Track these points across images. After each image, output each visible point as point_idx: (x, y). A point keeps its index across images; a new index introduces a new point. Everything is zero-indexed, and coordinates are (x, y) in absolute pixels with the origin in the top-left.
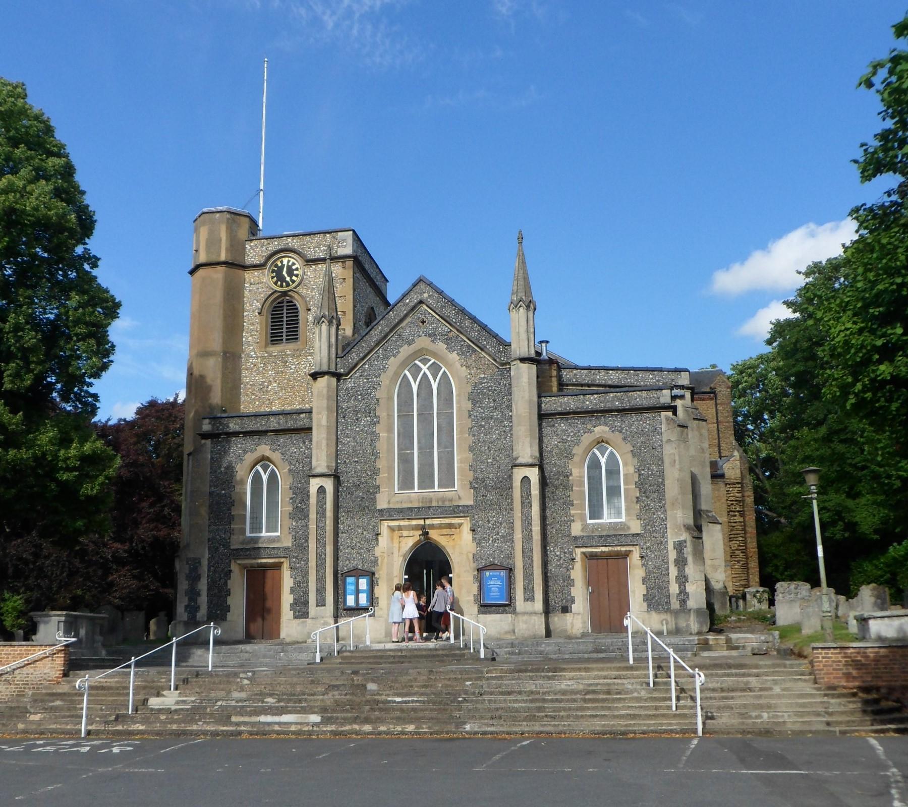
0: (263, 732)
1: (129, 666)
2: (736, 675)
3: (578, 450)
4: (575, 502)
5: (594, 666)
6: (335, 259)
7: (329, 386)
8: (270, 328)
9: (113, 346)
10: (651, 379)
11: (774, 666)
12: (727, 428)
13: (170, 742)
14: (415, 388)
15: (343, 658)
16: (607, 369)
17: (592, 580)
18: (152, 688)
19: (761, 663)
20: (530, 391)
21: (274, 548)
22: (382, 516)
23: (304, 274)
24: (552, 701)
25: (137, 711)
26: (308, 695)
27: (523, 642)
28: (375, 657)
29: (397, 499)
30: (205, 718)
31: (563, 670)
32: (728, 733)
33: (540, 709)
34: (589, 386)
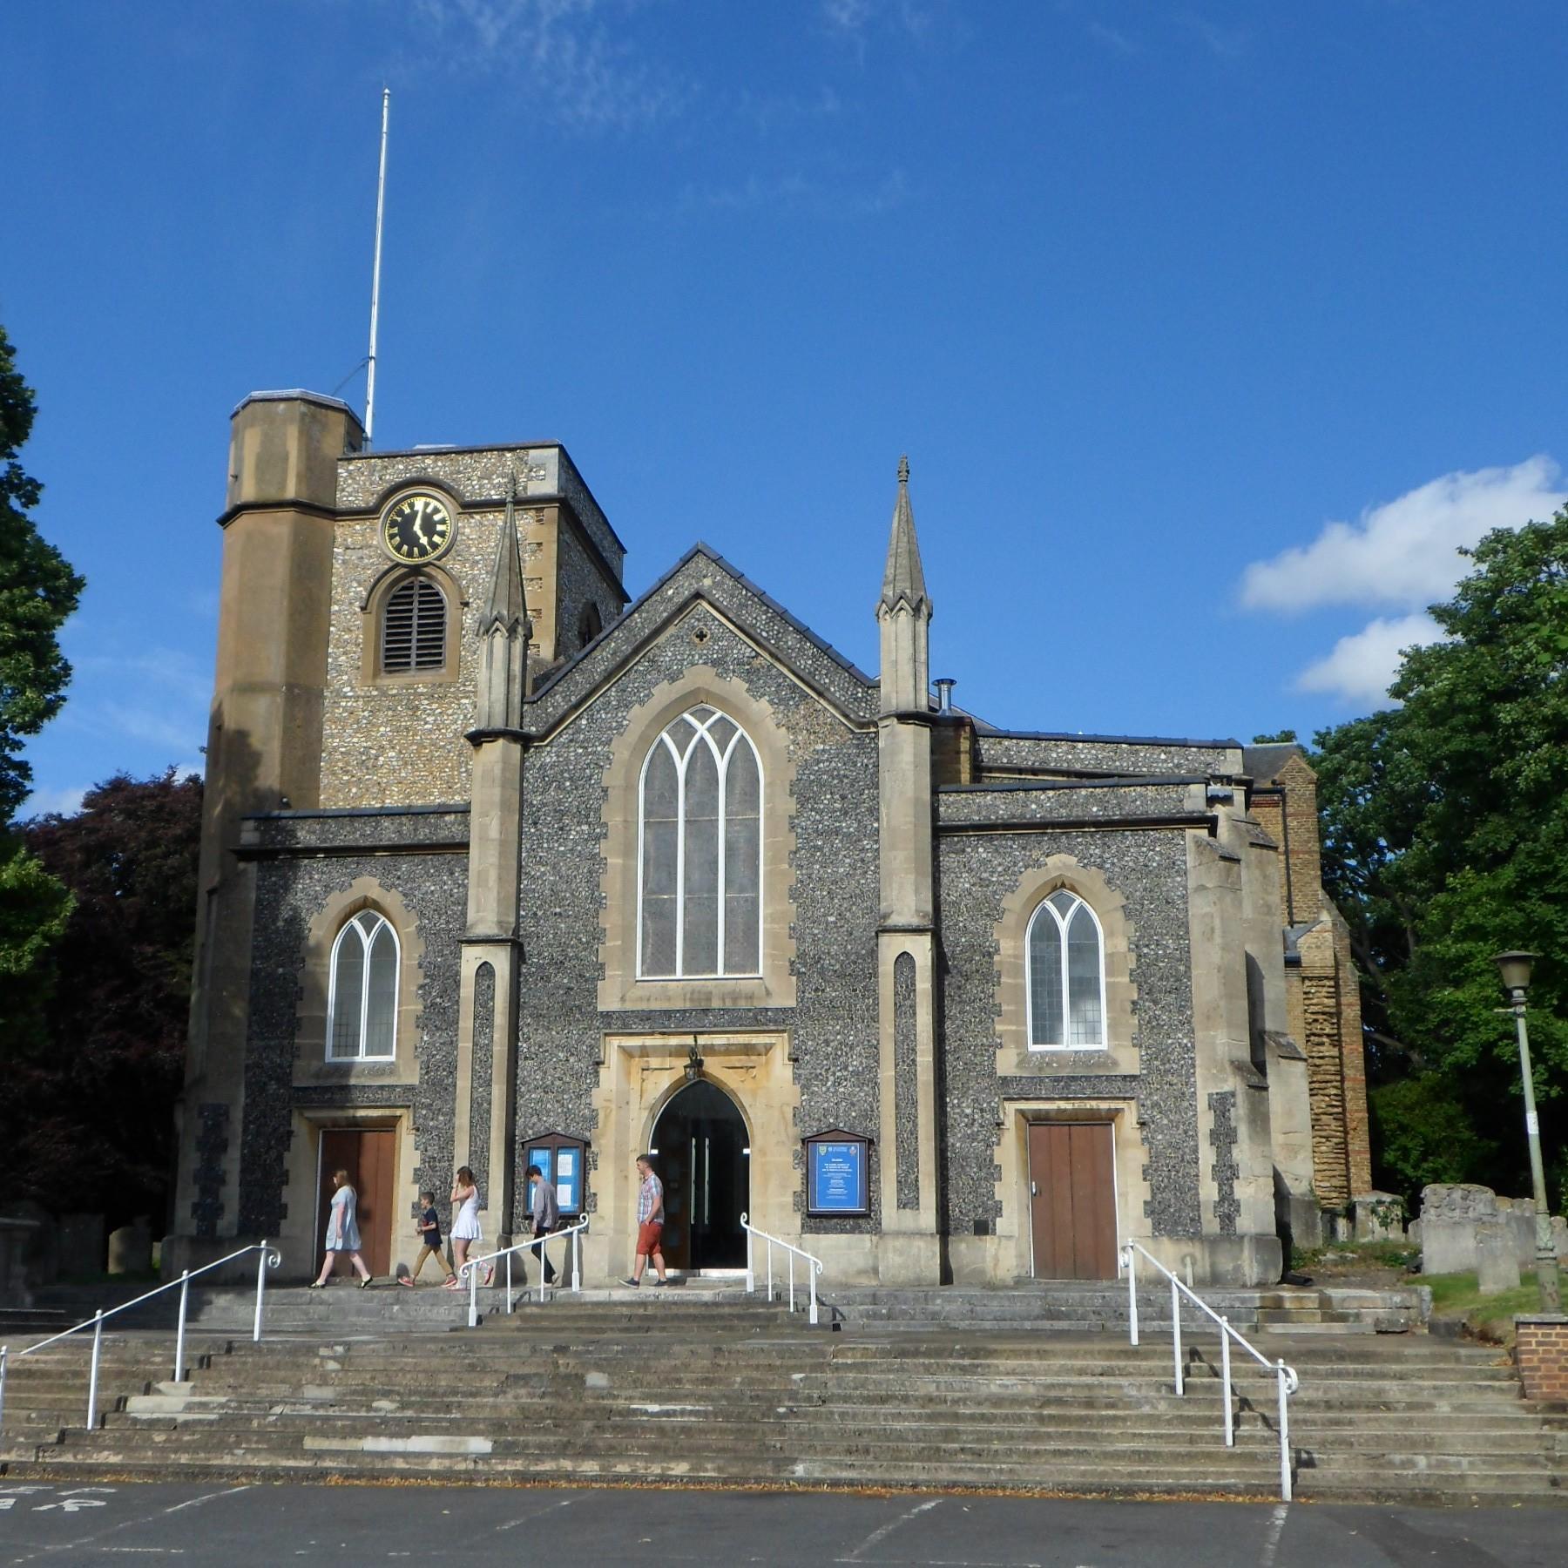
0: (371, 1472)
1: (91, 1328)
2: (1357, 1375)
5: (1058, 1346)
6: (522, 503)
7: (505, 761)
8: (383, 638)
9: (67, 668)
10: (1162, 762)
11: (1435, 1358)
12: (1305, 864)
13: (170, 1489)
14: (681, 767)
15: (524, 1318)
16: (1074, 740)
17: (1039, 1170)
18: (134, 1375)
19: (1408, 1351)
21: (382, 1087)
23: (457, 533)
24: (972, 1418)
25: (103, 1423)
26: (465, 1395)
27: (896, 1292)
28: (591, 1317)
30: (248, 1441)
31: (991, 1354)
32: (1347, 1497)
33: (948, 1435)
34: (1034, 772)
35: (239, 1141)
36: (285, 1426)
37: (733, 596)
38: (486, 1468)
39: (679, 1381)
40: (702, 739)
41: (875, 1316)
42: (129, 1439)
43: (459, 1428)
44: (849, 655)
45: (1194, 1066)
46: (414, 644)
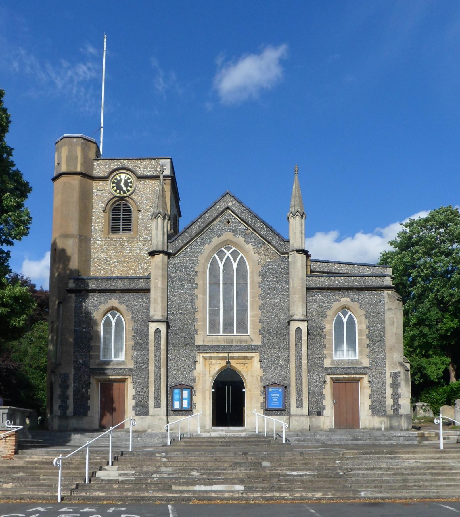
3: (329, 313)
4: (327, 346)
7: (163, 261)
8: (111, 221)
15: (185, 442)
16: (340, 263)
17: (336, 396)
21: (121, 369)
22: (199, 350)
29: (209, 339)
35: (73, 385)
37: (239, 209)
39: (296, 464)
40: (228, 257)
41: (299, 441)
43: (227, 482)
44: (278, 231)
45: (385, 364)
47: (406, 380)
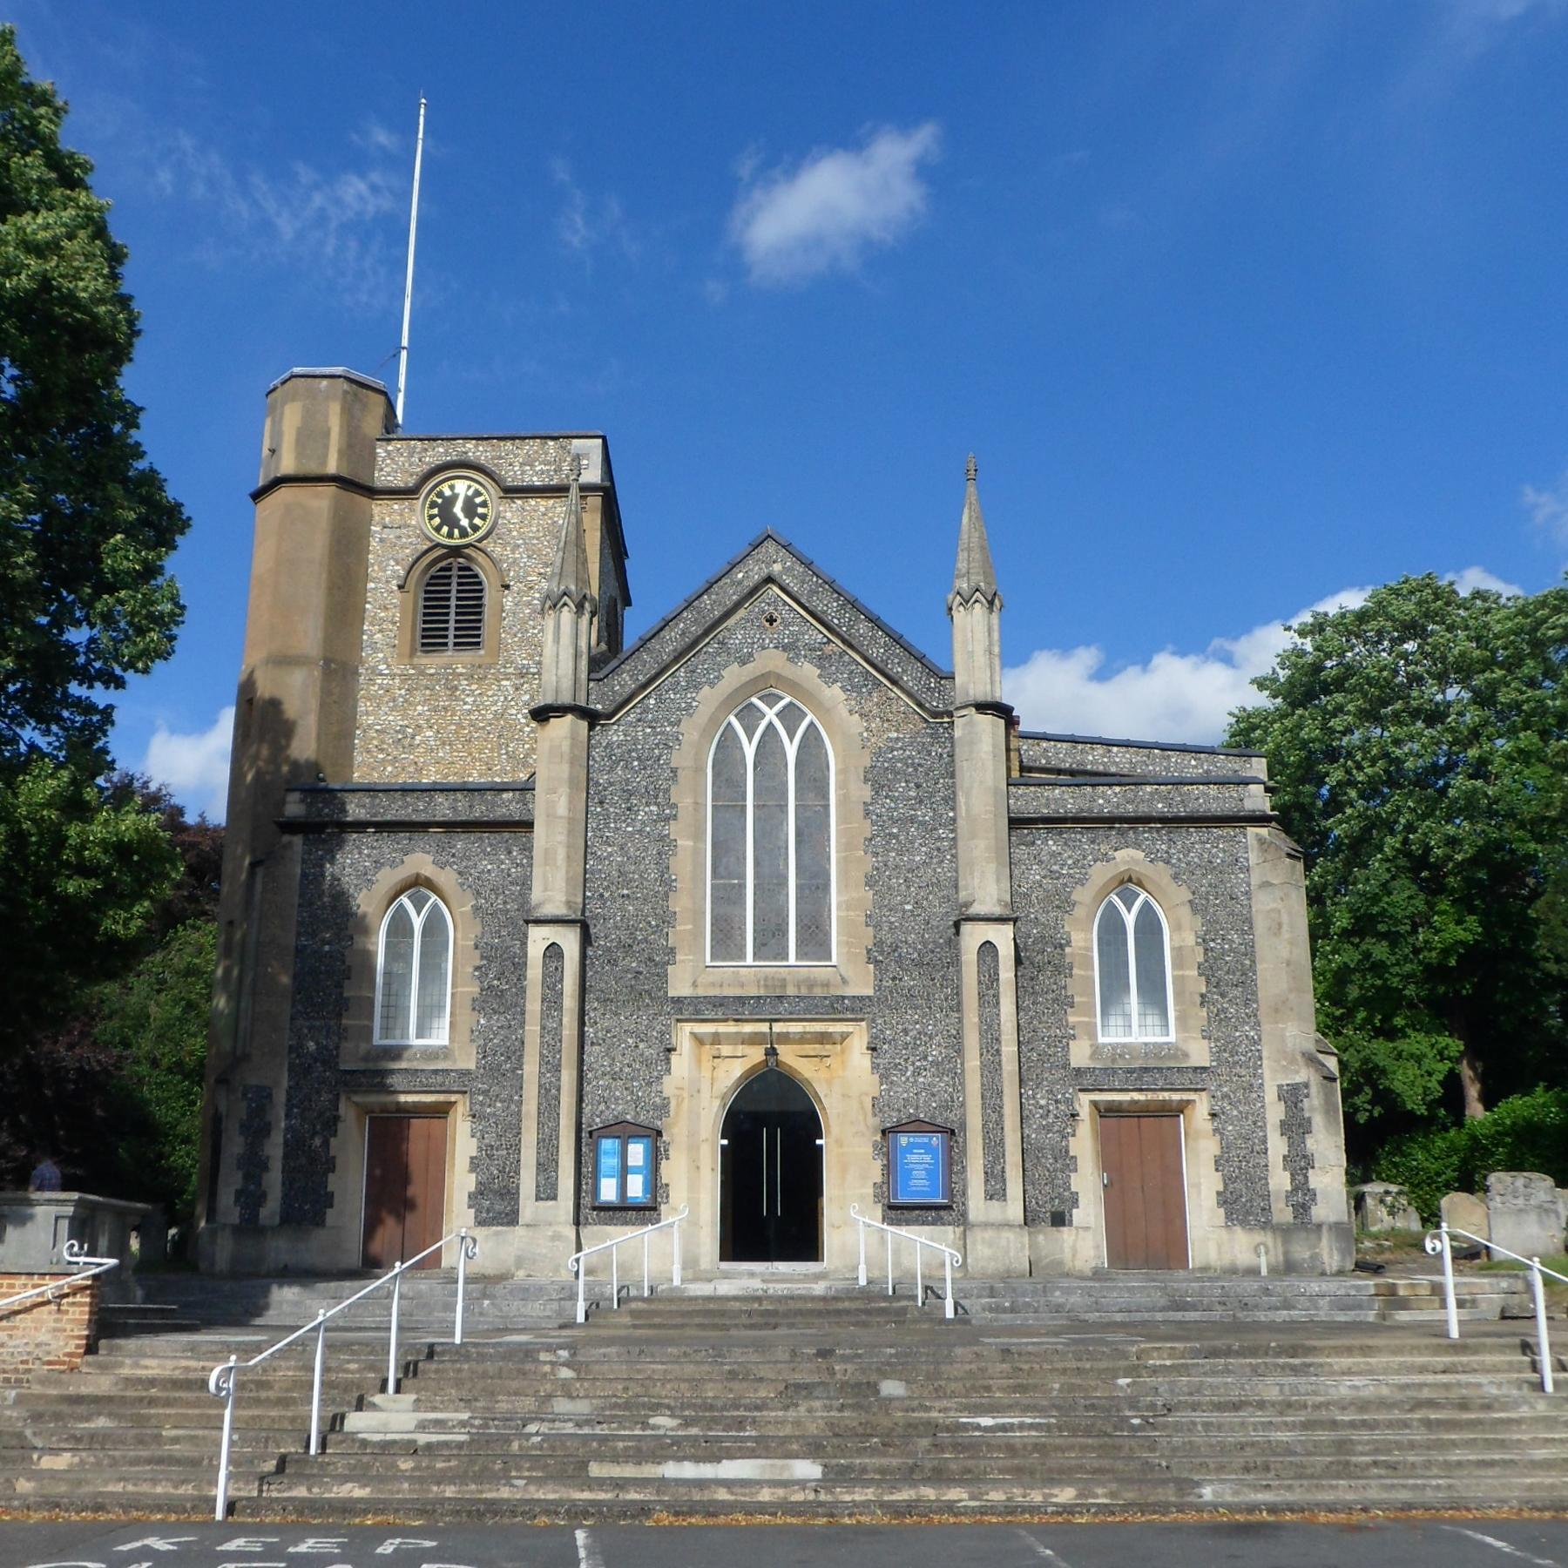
0: (690, 1503)
3: (1082, 895)
4: (1076, 999)
7: (574, 737)
8: (420, 618)
16: (1109, 744)
17: (1110, 1161)
20: (995, 770)
21: (436, 1072)
22: (680, 1011)
28: (707, 1313)
29: (711, 979)
36: (553, 1448)
37: (803, 582)
38: (829, 1498)
39: (988, 1389)
40: (770, 724)
41: (998, 1309)
42: (368, 1466)
43: (767, 1448)
44: (921, 646)
46: (452, 625)
47: (1329, 1109)
